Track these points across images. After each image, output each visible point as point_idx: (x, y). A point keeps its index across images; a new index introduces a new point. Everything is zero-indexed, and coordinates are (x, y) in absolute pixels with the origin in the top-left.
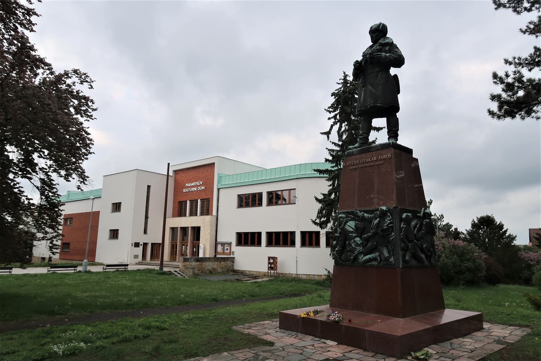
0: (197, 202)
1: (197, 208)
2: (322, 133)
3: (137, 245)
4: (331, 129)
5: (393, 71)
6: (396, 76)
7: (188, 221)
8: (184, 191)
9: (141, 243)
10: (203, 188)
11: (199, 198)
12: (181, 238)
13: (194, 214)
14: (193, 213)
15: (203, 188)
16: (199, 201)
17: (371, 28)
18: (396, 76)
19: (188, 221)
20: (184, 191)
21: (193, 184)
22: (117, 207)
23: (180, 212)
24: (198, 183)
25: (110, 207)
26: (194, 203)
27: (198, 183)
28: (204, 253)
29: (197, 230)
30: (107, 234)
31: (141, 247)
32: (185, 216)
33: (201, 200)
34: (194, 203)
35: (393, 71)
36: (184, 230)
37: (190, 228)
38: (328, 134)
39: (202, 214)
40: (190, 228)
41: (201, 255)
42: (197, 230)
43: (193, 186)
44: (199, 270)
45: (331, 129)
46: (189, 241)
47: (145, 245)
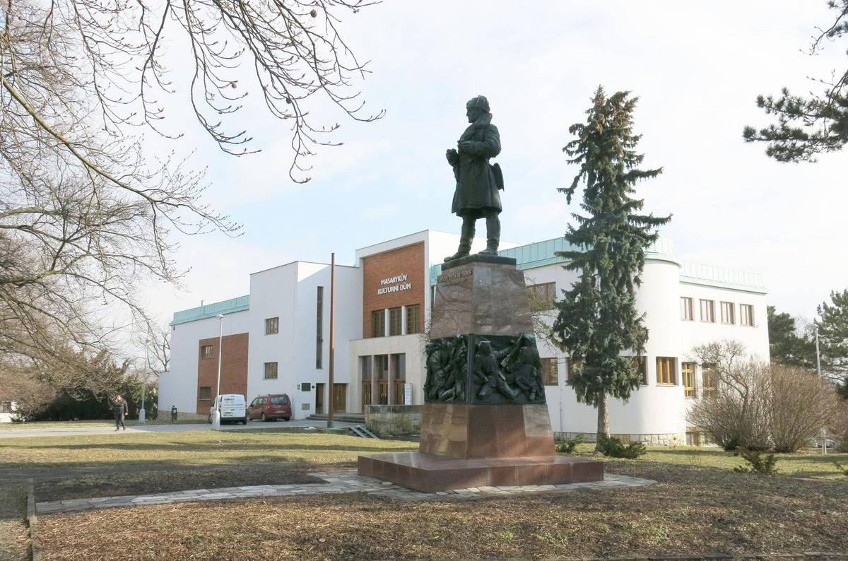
0: (384, 313)
1: (409, 320)
2: (560, 190)
3: (306, 387)
4: (575, 185)
5: (492, 161)
6: (497, 165)
7: (385, 345)
8: (379, 292)
9: (313, 384)
10: (408, 286)
11: (403, 303)
12: (377, 375)
13: (396, 332)
14: (395, 331)
15: (408, 286)
16: (403, 309)
17: (467, 104)
18: (497, 165)
19: (385, 345)
20: (379, 292)
21: (392, 281)
22: (272, 326)
23: (374, 328)
24: (399, 279)
25: (263, 325)
26: (395, 312)
27: (399, 279)
28: (413, 399)
29: (398, 358)
30: (262, 370)
31: (313, 391)
32: (383, 335)
33: (406, 306)
34: (395, 312)
35: (492, 161)
36: (381, 359)
37: (373, 359)
38: (569, 192)
39: (409, 332)
40: (389, 357)
41: (408, 402)
42: (398, 358)
43: (394, 284)
44: (398, 427)
45: (575, 185)
46: (389, 380)
47: (320, 387)
